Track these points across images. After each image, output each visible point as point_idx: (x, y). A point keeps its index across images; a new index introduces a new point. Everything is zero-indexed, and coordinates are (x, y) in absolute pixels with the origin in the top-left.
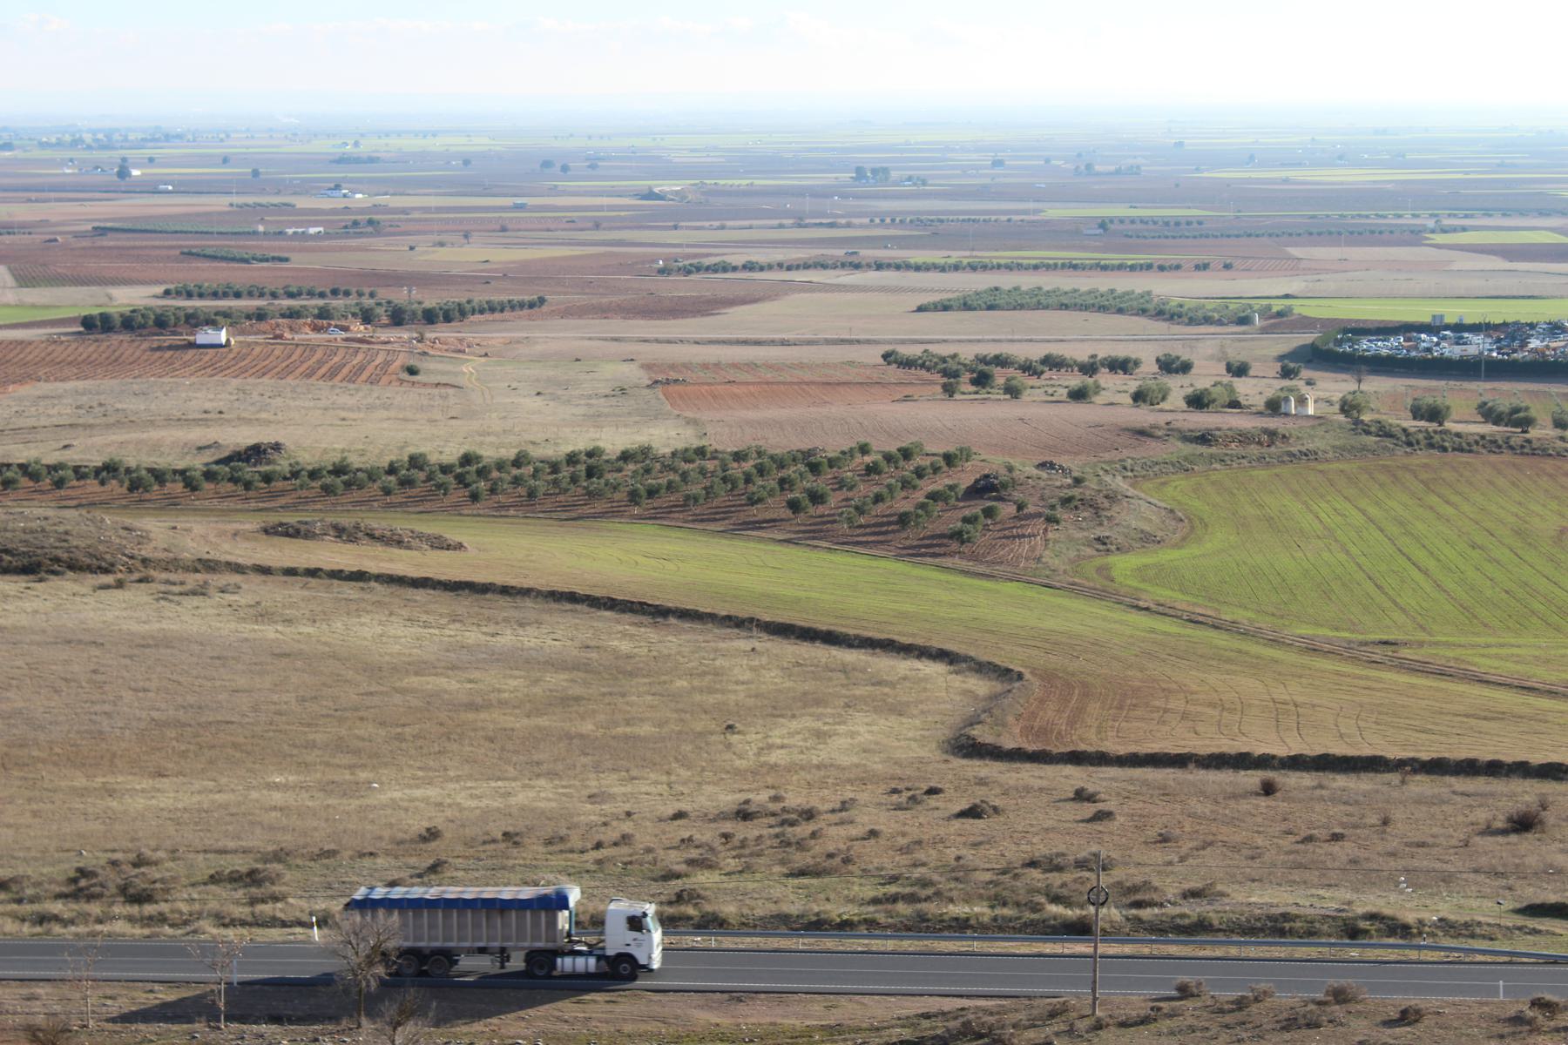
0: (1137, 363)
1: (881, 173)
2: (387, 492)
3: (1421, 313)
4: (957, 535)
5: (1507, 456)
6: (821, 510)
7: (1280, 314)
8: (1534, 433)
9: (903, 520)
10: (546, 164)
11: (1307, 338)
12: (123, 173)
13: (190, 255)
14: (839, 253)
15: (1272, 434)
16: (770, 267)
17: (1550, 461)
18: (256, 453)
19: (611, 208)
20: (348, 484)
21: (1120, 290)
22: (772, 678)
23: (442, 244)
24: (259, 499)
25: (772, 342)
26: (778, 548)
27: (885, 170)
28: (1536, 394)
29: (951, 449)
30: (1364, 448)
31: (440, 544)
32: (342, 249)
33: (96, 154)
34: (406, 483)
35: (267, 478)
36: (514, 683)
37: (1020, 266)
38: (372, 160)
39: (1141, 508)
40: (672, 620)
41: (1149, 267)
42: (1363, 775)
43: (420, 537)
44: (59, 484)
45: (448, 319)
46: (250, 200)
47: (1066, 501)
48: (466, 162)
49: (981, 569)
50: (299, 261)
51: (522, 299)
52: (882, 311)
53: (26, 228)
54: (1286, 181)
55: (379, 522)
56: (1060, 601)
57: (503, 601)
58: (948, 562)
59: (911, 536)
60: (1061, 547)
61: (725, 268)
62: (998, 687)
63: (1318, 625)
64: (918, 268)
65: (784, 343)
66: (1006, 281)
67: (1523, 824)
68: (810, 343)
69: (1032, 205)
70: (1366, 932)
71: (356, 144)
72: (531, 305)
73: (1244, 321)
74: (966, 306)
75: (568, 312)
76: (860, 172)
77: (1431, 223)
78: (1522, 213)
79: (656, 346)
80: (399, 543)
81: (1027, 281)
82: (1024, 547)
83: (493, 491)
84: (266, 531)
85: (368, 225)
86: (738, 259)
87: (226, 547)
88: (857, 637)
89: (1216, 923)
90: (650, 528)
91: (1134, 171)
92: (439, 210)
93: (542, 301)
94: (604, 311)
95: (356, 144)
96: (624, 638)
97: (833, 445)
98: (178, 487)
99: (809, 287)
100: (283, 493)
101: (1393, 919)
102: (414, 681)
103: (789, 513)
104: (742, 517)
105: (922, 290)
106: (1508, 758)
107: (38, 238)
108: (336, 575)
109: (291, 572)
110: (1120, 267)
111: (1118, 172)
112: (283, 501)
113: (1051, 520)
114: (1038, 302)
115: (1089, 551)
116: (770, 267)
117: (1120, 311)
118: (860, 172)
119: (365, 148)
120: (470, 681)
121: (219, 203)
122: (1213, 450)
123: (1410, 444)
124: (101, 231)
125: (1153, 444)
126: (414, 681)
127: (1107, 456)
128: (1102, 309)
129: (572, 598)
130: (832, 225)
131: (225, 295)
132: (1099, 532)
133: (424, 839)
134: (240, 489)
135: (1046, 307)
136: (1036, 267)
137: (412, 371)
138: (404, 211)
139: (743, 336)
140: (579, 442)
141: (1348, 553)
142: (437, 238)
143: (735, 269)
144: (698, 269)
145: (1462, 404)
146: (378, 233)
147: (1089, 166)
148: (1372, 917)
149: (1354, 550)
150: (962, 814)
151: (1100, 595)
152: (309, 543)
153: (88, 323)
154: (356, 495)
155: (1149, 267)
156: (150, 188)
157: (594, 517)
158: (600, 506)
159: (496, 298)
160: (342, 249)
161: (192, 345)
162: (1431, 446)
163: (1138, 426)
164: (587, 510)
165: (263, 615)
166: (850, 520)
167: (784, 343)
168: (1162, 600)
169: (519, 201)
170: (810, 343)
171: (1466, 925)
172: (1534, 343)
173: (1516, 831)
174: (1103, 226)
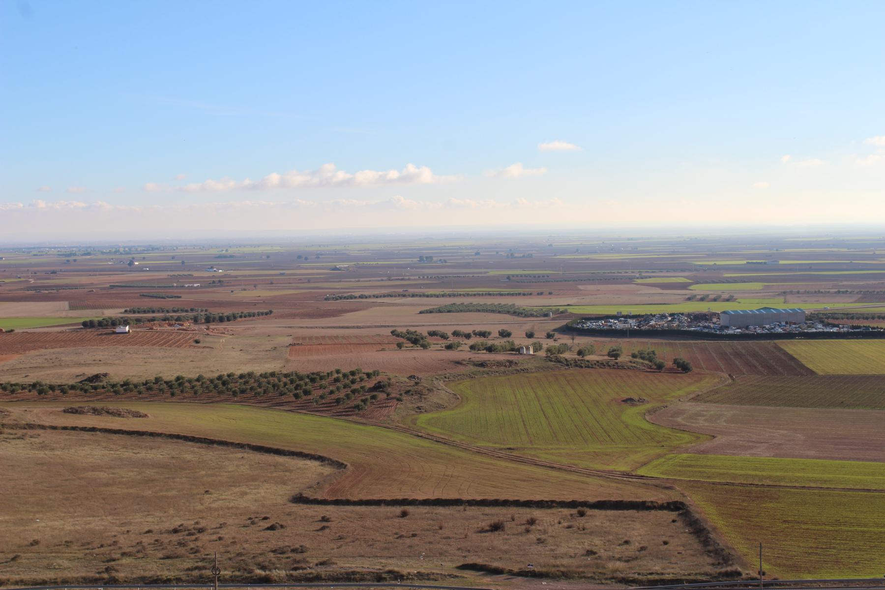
0: (489, 333)
1: (429, 258)
2: (140, 393)
3: (613, 311)
4: (357, 407)
5: (607, 369)
6: (309, 397)
7: (562, 312)
8: (620, 359)
9: (338, 401)
10: (299, 257)
11: (563, 323)
12: (131, 263)
13: (143, 296)
14: (400, 290)
15: (511, 362)
16: (370, 297)
17: (624, 371)
18: (97, 377)
19: (318, 274)
20: (125, 390)
21: (503, 303)
22: (245, 470)
23: (245, 290)
24: (89, 397)
25: (354, 327)
26: (285, 414)
27: (431, 257)
28: (658, 344)
29: (370, 371)
30: (548, 367)
31: (137, 415)
32: (209, 292)
33: (123, 256)
34: (149, 389)
35: (95, 388)
36: (131, 474)
37: (468, 295)
38: (231, 256)
39: (443, 392)
40: (215, 446)
41: (520, 294)
42: (451, 507)
43: (129, 412)
44: (13, 392)
45: (229, 320)
46: (176, 273)
47: (407, 392)
48: (268, 257)
49: (364, 421)
50: (186, 298)
51: (264, 311)
52: (406, 315)
53: (83, 286)
54: (587, 259)
55: (111, 407)
56: (389, 434)
57: (149, 439)
58: (350, 418)
59: (340, 408)
60: (396, 413)
61: (351, 297)
62: (336, 470)
63: (489, 441)
64: (428, 296)
65: (358, 327)
66: (458, 301)
67: (496, 527)
68: (369, 327)
69: (483, 270)
70: (385, 579)
71: (227, 250)
72: (266, 314)
73: (546, 315)
74: (440, 311)
75: (282, 316)
76: (421, 258)
77: (638, 275)
78: (675, 270)
79: (306, 329)
80: (119, 415)
81: (467, 301)
82: (385, 411)
83: (265, 392)
84: (64, 411)
85: (219, 282)
86: (357, 294)
87: (44, 418)
88: (288, 451)
89: (323, 576)
90: (237, 406)
91: (530, 256)
92: (250, 276)
93: (271, 312)
94: (293, 316)
95: (227, 250)
96: (191, 453)
97: (325, 370)
98: (58, 392)
99: (375, 304)
100: (101, 394)
101: (398, 572)
102: (90, 474)
103: (294, 399)
104: (277, 401)
105: (422, 305)
106: (511, 498)
107: (86, 290)
108: (84, 429)
109: (65, 428)
110: (508, 294)
111: (524, 256)
112: (99, 397)
113: (399, 400)
114: (468, 309)
115: (413, 412)
116: (370, 297)
117: (499, 312)
118: (421, 258)
119: (231, 251)
120: (113, 474)
121: (164, 275)
122: (485, 369)
123: (567, 365)
124: (112, 287)
125: (461, 367)
126: (90, 474)
127: (440, 373)
128: (493, 311)
129: (178, 437)
130: (402, 280)
131: (149, 312)
132: (419, 405)
133: (32, 545)
134: (82, 393)
135: (471, 311)
136: (475, 295)
137: (197, 342)
138: (236, 277)
139: (346, 325)
140: (245, 369)
141: (520, 411)
142: (244, 287)
143: (356, 298)
144: (341, 298)
145: (628, 347)
146: (221, 286)
147: (512, 255)
148: (390, 572)
149: (523, 409)
150: (268, 529)
151: (406, 431)
152: (81, 416)
153: (85, 324)
154: (129, 394)
155: (520, 294)
156: (140, 269)
157: (217, 402)
158: (223, 397)
159: (252, 311)
160: (209, 292)
161: (114, 333)
162: (576, 366)
163: (457, 360)
164: (218, 399)
165: (43, 447)
166: (316, 401)
167: (358, 327)
168: (430, 432)
169: (282, 272)
170: (369, 327)
171: (428, 574)
172: (652, 323)
173: (492, 531)
174: (508, 278)
